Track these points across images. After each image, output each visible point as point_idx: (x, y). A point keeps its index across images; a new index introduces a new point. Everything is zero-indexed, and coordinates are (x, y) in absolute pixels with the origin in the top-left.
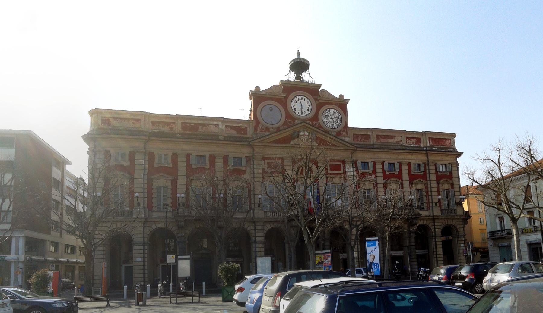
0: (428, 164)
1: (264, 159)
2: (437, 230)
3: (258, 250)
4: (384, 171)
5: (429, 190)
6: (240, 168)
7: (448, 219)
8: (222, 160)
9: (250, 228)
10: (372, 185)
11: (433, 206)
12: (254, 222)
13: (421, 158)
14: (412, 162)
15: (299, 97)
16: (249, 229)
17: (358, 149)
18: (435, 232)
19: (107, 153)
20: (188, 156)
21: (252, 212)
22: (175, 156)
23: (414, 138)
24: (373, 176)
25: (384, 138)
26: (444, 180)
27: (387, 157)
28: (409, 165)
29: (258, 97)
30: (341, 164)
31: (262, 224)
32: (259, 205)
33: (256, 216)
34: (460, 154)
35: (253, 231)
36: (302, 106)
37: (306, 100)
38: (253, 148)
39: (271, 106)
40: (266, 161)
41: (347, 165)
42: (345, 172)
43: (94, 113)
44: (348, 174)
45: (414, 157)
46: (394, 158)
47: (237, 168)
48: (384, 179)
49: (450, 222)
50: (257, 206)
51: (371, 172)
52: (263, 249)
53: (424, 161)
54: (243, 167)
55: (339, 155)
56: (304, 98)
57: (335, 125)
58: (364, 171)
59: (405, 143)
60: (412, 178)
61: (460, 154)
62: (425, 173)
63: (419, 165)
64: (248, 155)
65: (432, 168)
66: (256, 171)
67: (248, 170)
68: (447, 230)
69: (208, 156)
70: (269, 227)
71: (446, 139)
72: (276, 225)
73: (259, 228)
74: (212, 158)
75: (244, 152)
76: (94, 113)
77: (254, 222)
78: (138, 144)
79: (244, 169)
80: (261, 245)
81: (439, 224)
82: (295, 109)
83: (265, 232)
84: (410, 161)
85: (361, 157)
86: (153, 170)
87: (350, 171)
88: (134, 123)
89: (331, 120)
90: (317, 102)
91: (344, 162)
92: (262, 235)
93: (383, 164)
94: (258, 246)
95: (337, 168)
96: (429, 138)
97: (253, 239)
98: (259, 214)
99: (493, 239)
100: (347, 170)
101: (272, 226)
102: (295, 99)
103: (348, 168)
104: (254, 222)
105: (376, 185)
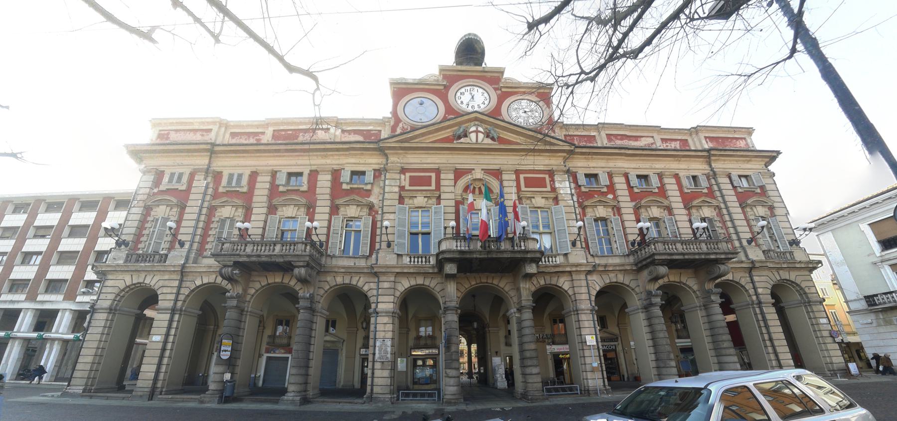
0: (715, 174)
1: (403, 171)
2: (760, 291)
3: (379, 327)
4: (630, 188)
5: (727, 218)
6: (361, 186)
7: (778, 269)
8: (329, 177)
9: (366, 285)
10: (610, 210)
11: (742, 246)
12: (375, 273)
13: (699, 168)
14: (682, 174)
15: (468, 88)
16: (366, 288)
17: (578, 150)
18: (757, 294)
19: (159, 175)
20: (274, 174)
21: (374, 256)
22: (254, 176)
23: (676, 140)
24: (610, 196)
25: (621, 139)
26: (755, 199)
27: (635, 167)
28: (676, 177)
29: (402, 90)
30: (547, 176)
31: (392, 279)
32: (389, 245)
33: (380, 262)
34: (772, 156)
35: (375, 292)
36: (474, 98)
37: (481, 90)
38: (315, 79)
39: (419, 99)
40: (408, 175)
41: (556, 178)
42: (554, 189)
43: (155, 124)
44: (562, 192)
45: (683, 165)
46: (649, 167)
47: (355, 186)
48: (632, 201)
49: (785, 275)
50: (384, 245)
51: (605, 190)
52: (390, 327)
53: (706, 172)
54: (366, 184)
55: (541, 162)
56: (476, 88)
57: (531, 121)
58: (589, 192)
59: (659, 144)
60: (688, 200)
61: (772, 156)
62: (710, 188)
63: (694, 177)
64: (377, 167)
65: (723, 180)
66: (387, 189)
67: (376, 190)
68: (778, 292)
69: (306, 172)
70: (405, 284)
71: (737, 139)
72: (420, 281)
73: (386, 285)
74: (314, 174)
75: (370, 162)
76: (155, 124)
77: (376, 274)
78: (202, 161)
79: (369, 187)
80: (386, 320)
81: (763, 279)
82: (462, 103)
83: (398, 294)
84: (677, 171)
85: (581, 165)
86: (219, 194)
87: (564, 187)
88: (202, 135)
89: (524, 115)
90: (499, 92)
91: (551, 173)
92: (391, 299)
93: (626, 176)
94: (380, 320)
95: (541, 183)
96: (706, 138)
97: (373, 306)
98: (386, 258)
99: (876, 312)
100: (557, 185)
101: (413, 283)
102: (463, 90)
103: (560, 182)
104: (376, 274)
105: (617, 210)
